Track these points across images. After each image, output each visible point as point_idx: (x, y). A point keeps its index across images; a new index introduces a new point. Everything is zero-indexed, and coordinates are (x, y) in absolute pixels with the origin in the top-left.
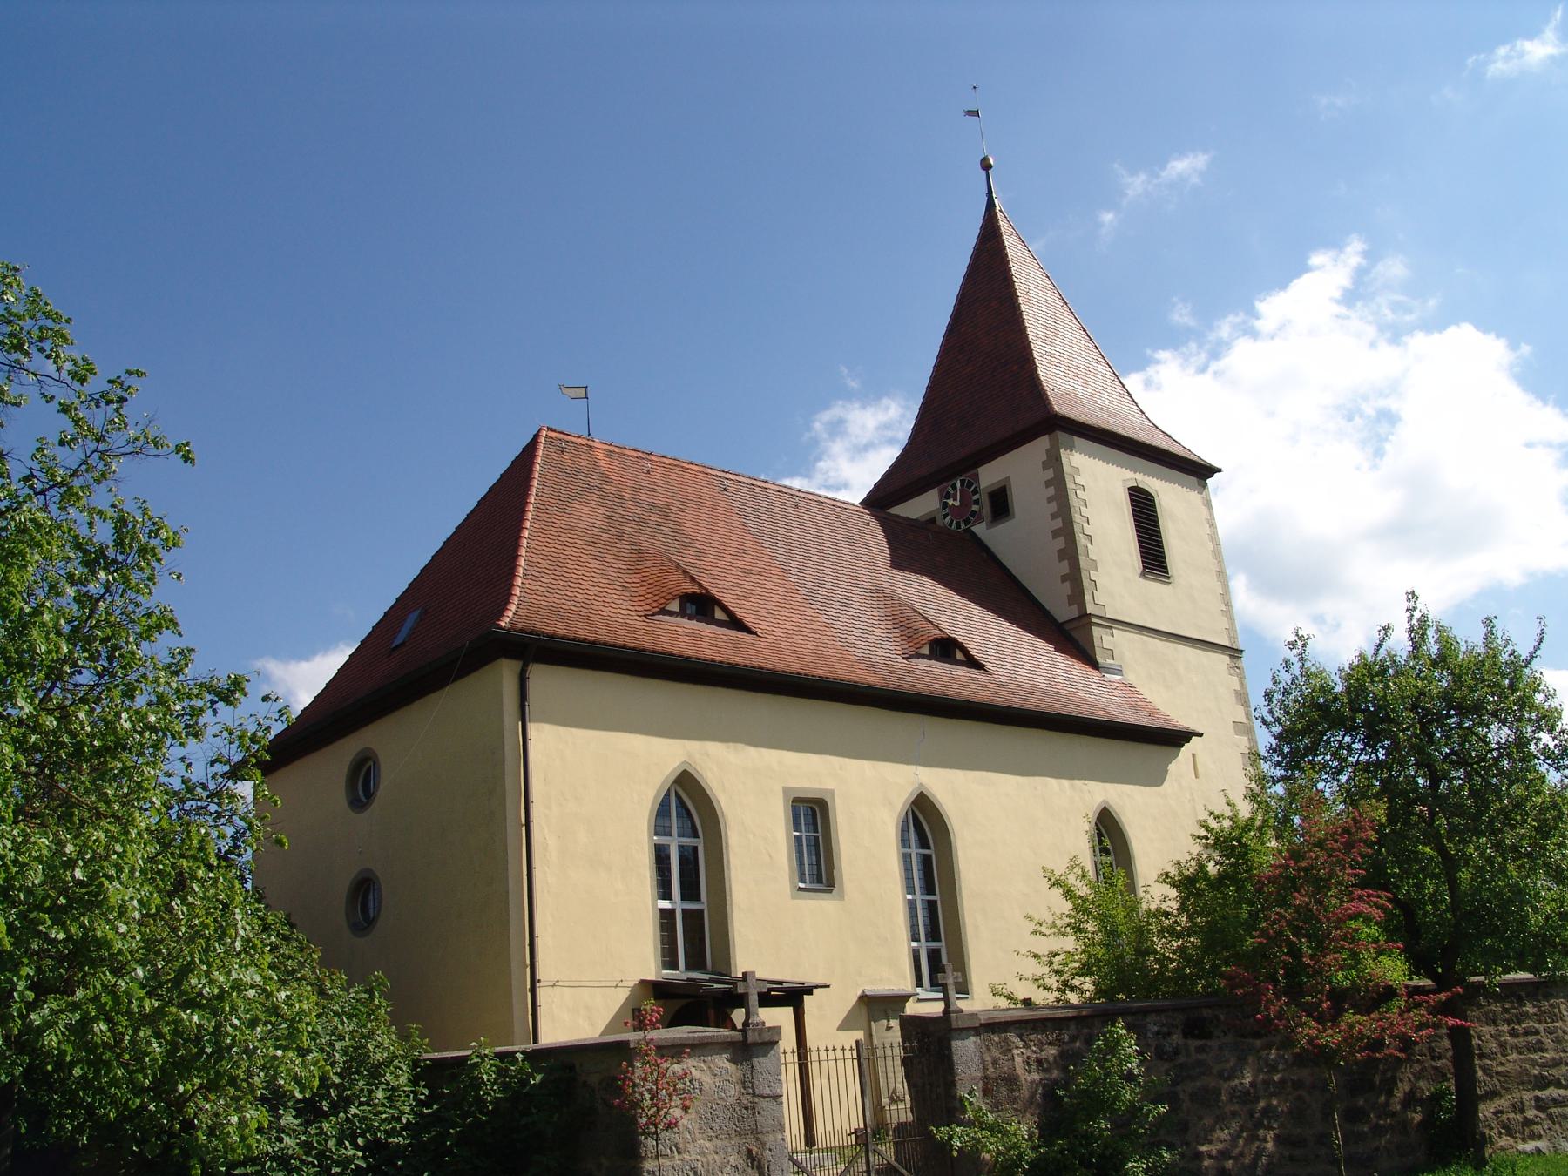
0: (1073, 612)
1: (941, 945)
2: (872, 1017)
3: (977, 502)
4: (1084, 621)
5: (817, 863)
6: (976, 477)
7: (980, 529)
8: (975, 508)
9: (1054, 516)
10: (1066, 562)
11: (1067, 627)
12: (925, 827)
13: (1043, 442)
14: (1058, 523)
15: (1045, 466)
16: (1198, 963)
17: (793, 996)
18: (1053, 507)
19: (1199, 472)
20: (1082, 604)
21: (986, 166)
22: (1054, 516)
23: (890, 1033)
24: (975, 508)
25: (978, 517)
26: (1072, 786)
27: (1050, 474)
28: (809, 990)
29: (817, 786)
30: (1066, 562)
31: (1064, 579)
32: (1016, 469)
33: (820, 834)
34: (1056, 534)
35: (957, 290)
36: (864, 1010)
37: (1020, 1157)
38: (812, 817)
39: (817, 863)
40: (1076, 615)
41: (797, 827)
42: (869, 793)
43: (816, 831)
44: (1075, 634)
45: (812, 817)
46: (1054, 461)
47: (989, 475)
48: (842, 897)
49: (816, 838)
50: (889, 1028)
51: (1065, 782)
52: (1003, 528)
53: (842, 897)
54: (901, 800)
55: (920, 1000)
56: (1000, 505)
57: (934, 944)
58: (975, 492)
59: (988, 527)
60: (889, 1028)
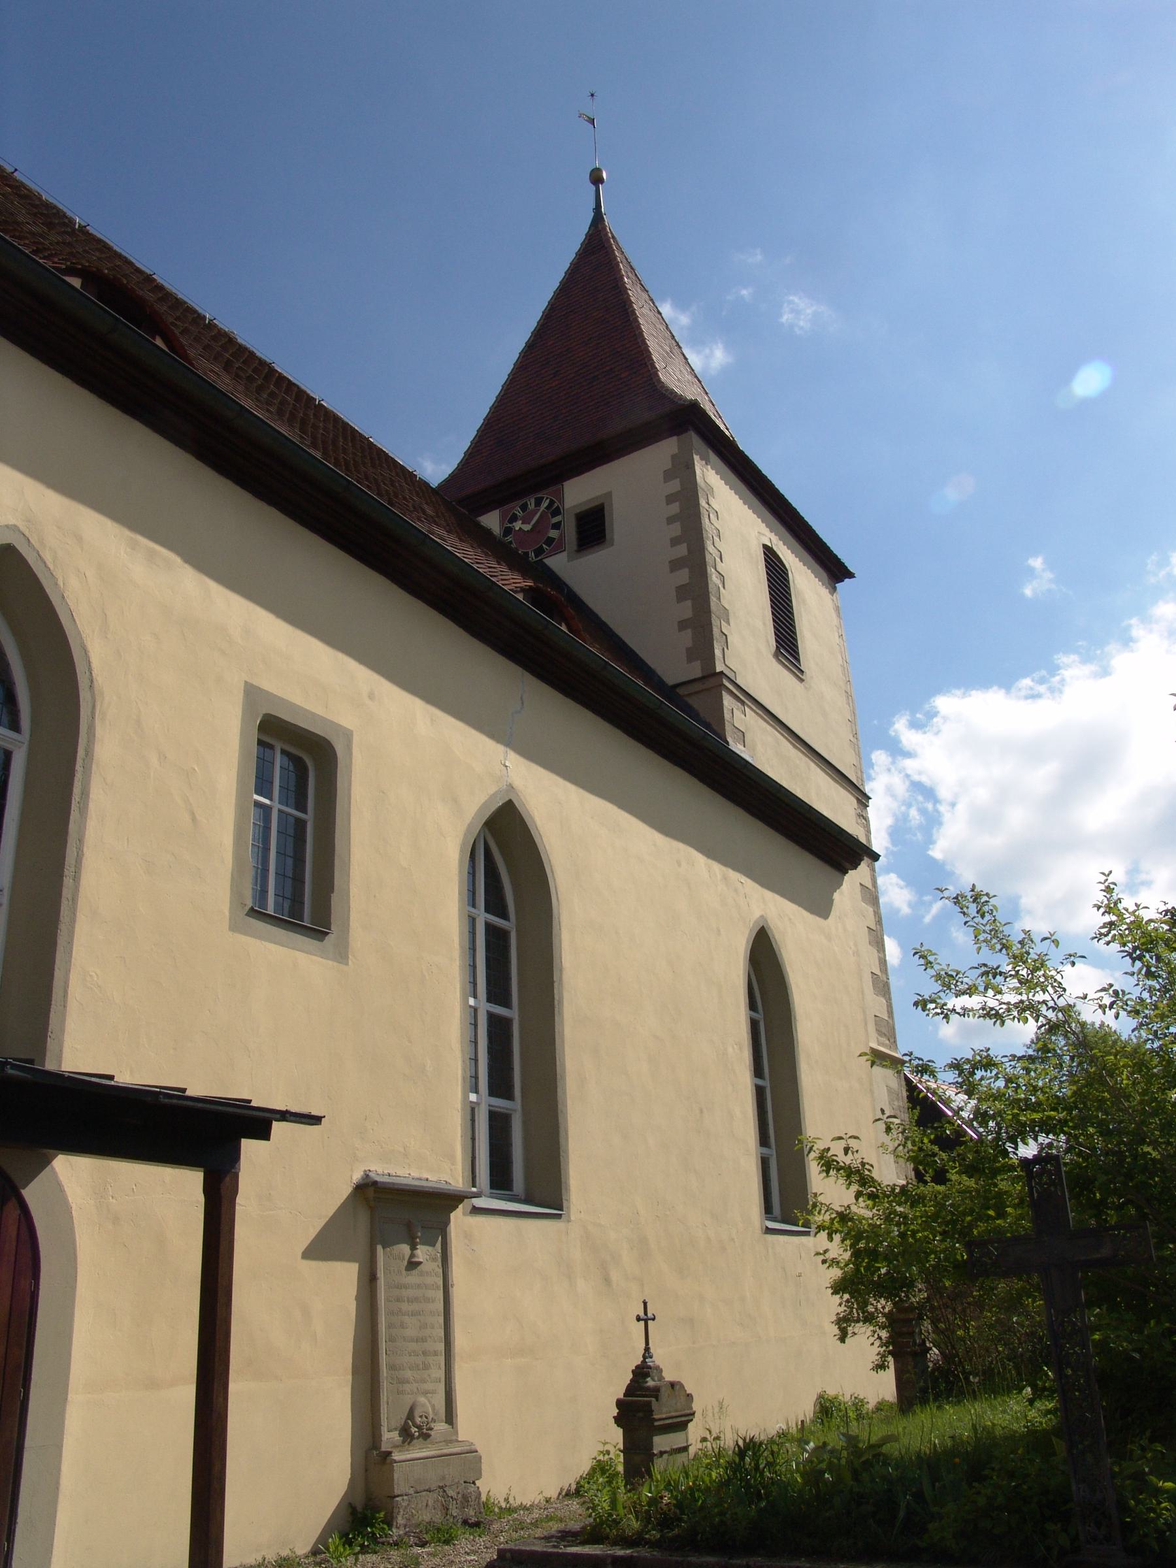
0: (696, 670)
1: (514, 1106)
2: (379, 1237)
3: (557, 526)
4: (711, 682)
5: (296, 872)
6: (560, 495)
7: (557, 563)
8: (553, 534)
9: (675, 542)
10: (689, 603)
11: (681, 691)
12: (506, 866)
13: (664, 450)
14: (682, 550)
15: (668, 476)
16: (1033, 1131)
17: (202, 1134)
18: (676, 529)
19: (834, 570)
20: (708, 657)
21: (596, 179)
22: (675, 542)
23: (413, 1278)
24: (553, 534)
25: (556, 546)
26: (725, 878)
27: (675, 486)
28: (257, 1122)
29: (319, 711)
30: (689, 603)
31: (683, 625)
32: (625, 485)
33: (309, 817)
34: (675, 565)
35: (566, 266)
36: (363, 1218)
37: (1153, 1520)
38: (297, 767)
39: (296, 872)
40: (698, 673)
41: (263, 785)
42: (427, 761)
43: (301, 806)
44: (694, 702)
45: (297, 767)
46: (683, 471)
47: (578, 492)
48: (342, 955)
49: (300, 825)
50: (413, 1265)
51: (717, 867)
52: (597, 558)
53: (342, 955)
54: (475, 804)
55: (476, 1211)
56: (593, 528)
57: (500, 1103)
58: (557, 512)
59: (570, 559)
60: (413, 1265)
